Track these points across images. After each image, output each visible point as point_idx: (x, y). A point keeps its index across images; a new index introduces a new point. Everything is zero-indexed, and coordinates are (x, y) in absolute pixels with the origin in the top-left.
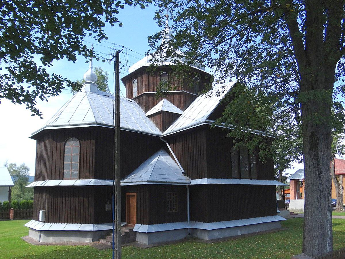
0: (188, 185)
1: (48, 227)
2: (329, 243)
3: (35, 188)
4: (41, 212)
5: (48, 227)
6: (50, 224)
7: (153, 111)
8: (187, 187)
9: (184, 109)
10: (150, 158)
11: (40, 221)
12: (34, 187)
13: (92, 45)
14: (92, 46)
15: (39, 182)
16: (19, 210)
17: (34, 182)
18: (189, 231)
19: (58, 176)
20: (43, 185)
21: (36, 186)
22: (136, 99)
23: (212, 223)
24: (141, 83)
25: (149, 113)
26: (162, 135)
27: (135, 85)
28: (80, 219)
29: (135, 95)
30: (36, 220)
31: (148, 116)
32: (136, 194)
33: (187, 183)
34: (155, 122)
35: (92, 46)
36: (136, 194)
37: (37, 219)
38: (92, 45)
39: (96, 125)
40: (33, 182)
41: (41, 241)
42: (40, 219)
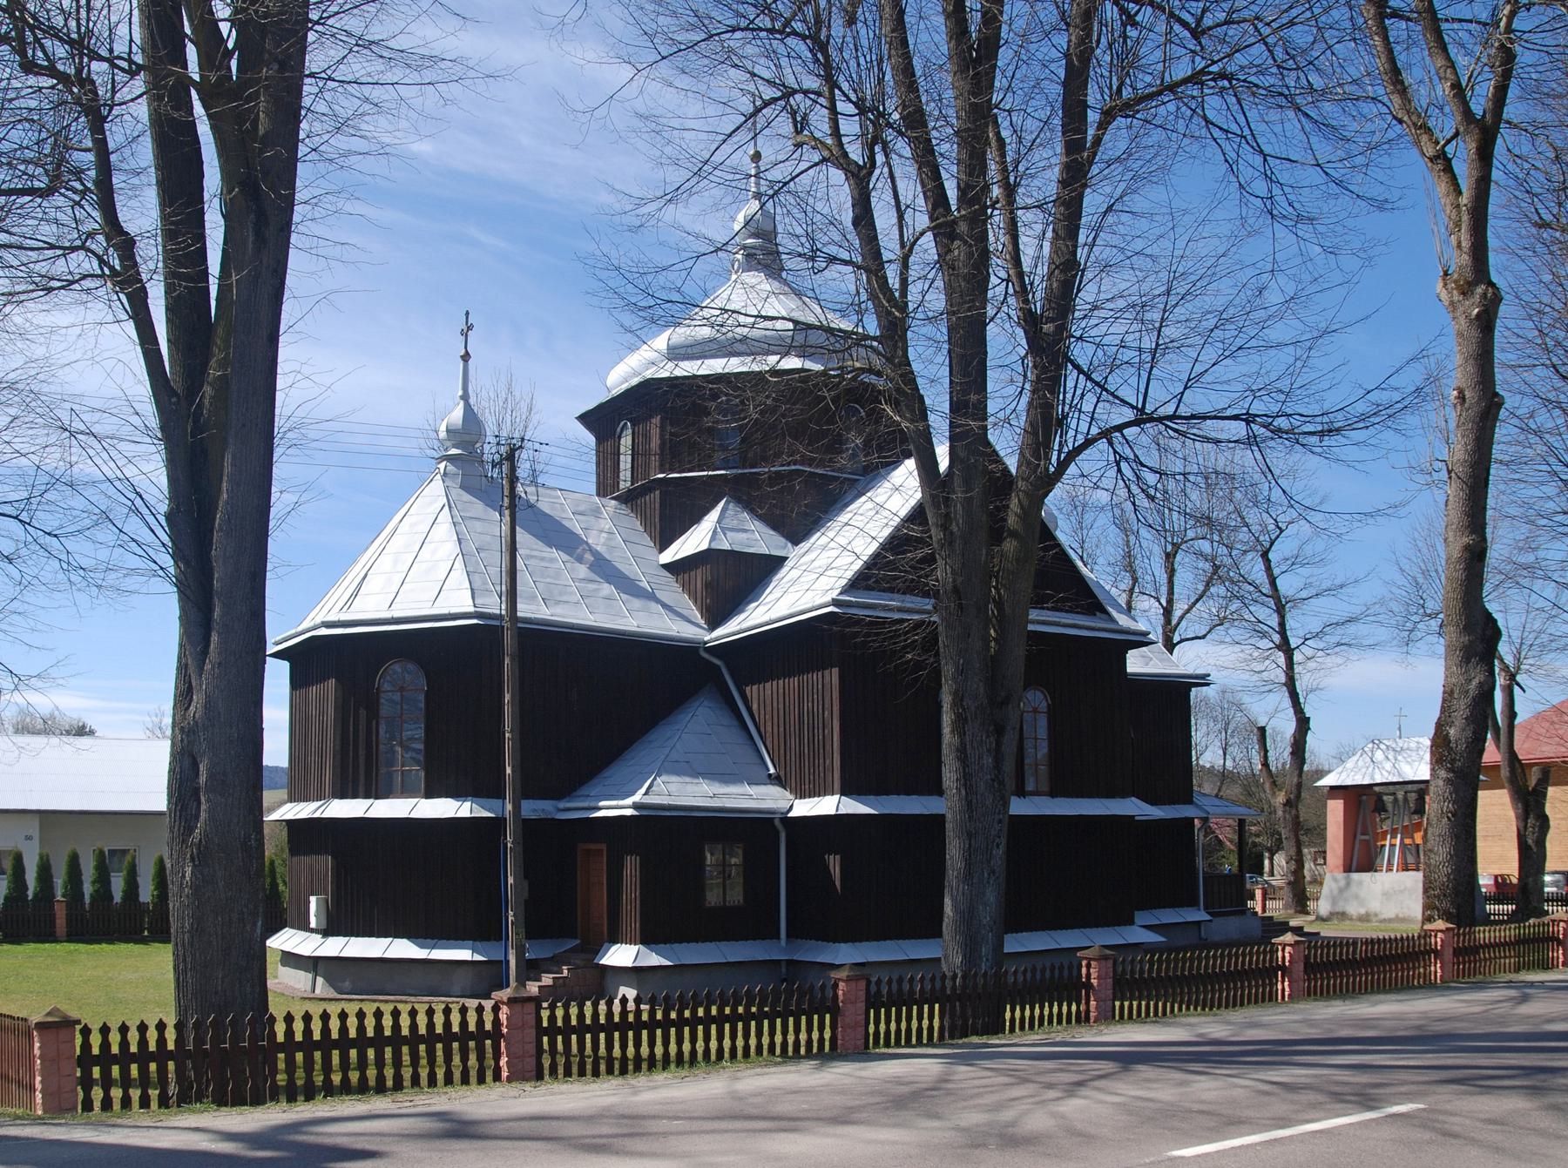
0: (781, 818)
1: (335, 947)
2: (987, 960)
3: (292, 825)
4: (313, 899)
5: (335, 947)
6: (341, 941)
7: (694, 541)
8: (777, 823)
9: (796, 538)
10: (664, 722)
11: (312, 931)
12: (289, 822)
13: (467, 313)
14: (467, 318)
15: (303, 805)
16: (784, 274)
17: (289, 805)
18: (784, 970)
19: (361, 789)
20: (317, 815)
21: (297, 817)
22: (628, 499)
23: (857, 944)
24: (647, 436)
25: (668, 556)
26: (706, 639)
27: (626, 442)
28: (642, 1122)
29: (625, 484)
30: (299, 929)
31: (666, 567)
32: (604, 846)
33: (774, 813)
34: (687, 588)
35: (467, 318)
36: (604, 846)
37: (303, 925)
38: (467, 313)
39: (475, 621)
40: (282, 804)
41: (318, 991)
42: (313, 924)
